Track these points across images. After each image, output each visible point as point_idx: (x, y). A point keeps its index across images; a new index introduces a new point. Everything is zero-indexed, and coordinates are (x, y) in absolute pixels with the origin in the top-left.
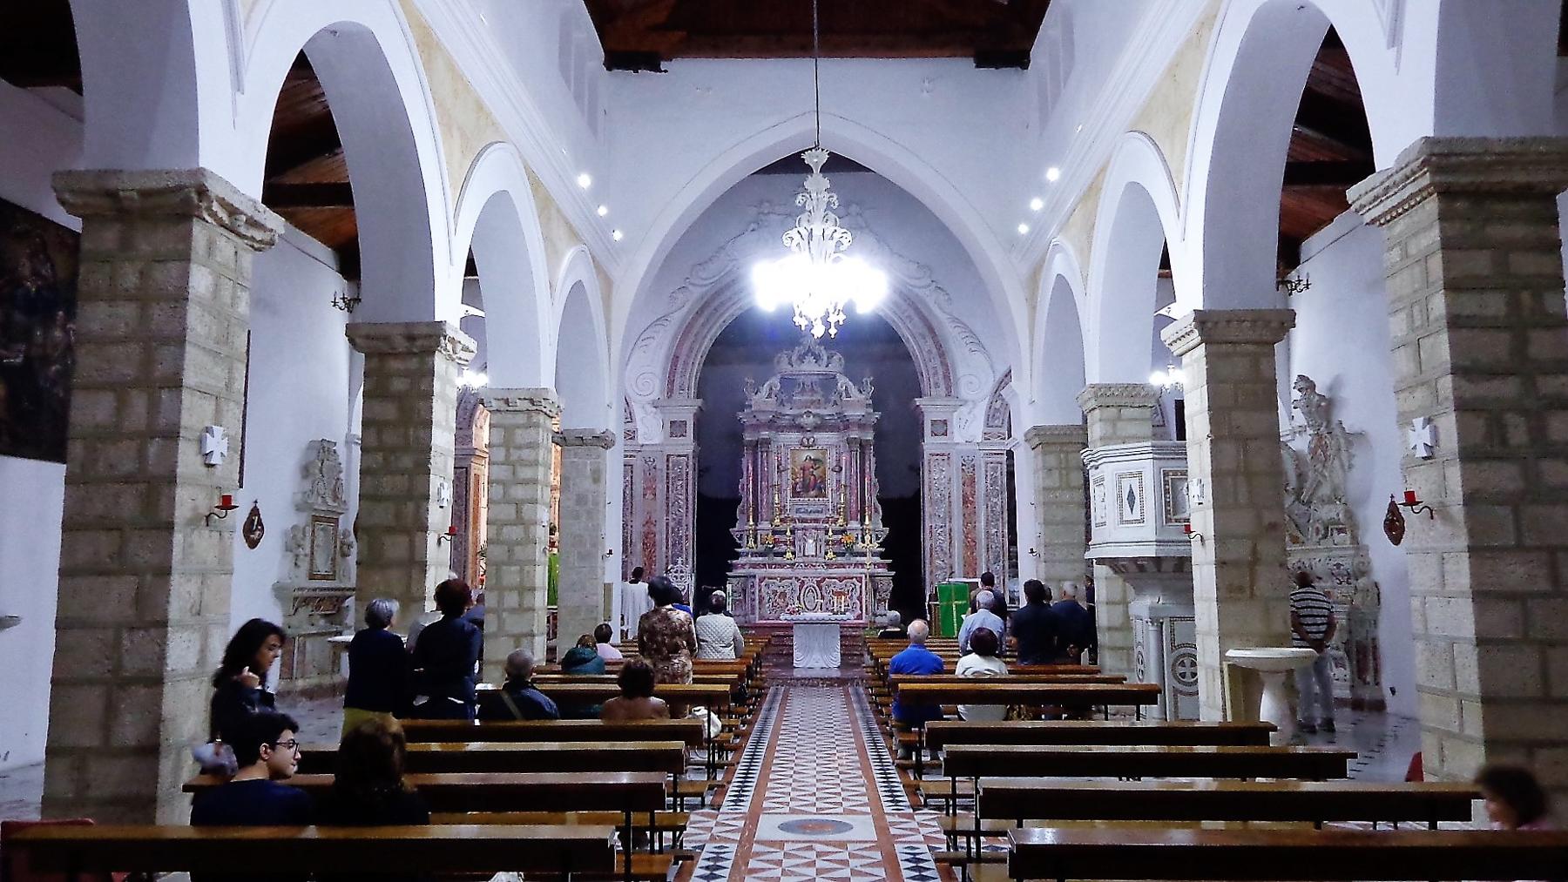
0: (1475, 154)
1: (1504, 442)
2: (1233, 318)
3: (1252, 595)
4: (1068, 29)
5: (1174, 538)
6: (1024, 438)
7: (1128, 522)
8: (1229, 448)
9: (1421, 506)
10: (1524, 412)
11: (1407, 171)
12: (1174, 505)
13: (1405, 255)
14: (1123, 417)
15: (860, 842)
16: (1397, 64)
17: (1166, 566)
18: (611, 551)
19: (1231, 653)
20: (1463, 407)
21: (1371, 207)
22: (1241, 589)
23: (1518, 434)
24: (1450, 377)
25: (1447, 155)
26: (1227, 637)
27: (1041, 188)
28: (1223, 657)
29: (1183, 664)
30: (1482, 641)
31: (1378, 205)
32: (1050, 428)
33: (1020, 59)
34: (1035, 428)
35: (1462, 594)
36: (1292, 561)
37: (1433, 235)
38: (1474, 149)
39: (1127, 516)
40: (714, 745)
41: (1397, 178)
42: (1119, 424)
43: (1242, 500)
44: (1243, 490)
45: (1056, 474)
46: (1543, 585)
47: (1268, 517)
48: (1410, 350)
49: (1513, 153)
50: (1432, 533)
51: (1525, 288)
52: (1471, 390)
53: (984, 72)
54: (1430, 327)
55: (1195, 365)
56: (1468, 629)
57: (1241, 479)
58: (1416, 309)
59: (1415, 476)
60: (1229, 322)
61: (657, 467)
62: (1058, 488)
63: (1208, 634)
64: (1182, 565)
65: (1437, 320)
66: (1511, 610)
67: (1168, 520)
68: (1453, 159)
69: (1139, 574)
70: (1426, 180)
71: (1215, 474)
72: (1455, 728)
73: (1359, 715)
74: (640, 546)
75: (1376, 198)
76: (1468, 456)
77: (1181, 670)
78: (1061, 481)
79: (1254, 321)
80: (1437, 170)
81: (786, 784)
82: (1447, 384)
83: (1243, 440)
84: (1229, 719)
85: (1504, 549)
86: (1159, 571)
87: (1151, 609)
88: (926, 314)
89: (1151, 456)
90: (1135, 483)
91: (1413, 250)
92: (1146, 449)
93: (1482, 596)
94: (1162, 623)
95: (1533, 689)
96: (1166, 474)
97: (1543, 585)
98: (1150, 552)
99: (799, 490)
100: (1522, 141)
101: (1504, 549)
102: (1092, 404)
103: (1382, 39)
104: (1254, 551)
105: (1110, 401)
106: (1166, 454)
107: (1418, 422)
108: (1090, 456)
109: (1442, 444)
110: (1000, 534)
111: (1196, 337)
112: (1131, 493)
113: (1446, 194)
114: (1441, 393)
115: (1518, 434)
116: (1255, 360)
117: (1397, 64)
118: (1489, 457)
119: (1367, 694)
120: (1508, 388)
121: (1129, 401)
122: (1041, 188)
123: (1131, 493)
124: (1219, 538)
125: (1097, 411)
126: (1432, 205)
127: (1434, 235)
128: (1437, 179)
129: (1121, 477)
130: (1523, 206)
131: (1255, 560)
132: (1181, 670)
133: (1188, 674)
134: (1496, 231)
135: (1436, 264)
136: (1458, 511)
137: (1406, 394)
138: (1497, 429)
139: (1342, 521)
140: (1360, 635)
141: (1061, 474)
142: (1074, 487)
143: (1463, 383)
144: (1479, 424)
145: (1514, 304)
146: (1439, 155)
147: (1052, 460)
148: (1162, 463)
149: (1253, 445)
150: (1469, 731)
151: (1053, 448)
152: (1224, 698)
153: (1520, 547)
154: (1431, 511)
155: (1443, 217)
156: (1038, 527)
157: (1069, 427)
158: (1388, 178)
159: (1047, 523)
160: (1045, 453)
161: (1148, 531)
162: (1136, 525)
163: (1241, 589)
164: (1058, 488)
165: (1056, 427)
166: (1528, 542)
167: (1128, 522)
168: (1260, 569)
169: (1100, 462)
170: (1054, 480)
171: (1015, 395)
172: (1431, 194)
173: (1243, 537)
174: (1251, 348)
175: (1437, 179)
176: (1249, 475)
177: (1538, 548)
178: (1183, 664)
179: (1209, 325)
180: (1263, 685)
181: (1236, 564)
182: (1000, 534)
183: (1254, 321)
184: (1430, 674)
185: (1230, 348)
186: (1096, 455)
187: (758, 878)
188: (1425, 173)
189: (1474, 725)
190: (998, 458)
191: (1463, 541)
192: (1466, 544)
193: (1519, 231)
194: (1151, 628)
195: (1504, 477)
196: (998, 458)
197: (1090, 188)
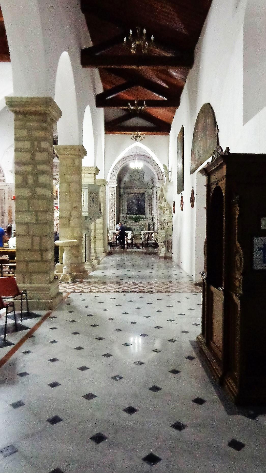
1: (27, 183)
3: (69, 227)
10: (32, 175)
18: (164, 219)
20: (17, 173)
22: (66, 224)
23: (31, 180)
36: (40, 217)
43: (68, 200)
44: (68, 197)
46: (34, 221)
47: (75, 204)
49: (28, 102)
51: (36, 140)
52: (20, 169)
57: (68, 194)
60: (64, 149)
61: (12, 190)
66: (25, 227)
73: (166, 261)
74: (7, 214)
79: (71, 149)
81: (121, 287)
85: (24, 211)
88: (180, 145)
95: (29, 248)
97: (34, 221)
99: (55, 198)
100: (32, 98)
101: (24, 211)
104: (70, 214)
110: (114, 211)
115: (31, 180)
118: (23, 187)
119: (169, 255)
120: (29, 168)
130: (37, 117)
134: (29, 124)
138: (25, 180)
139: (166, 207)
140: (168, 239)
143: (18, 167)
144: (20, 177)
145: (32, 144)
153: (28, 211)
163: (66, 224)
166: (31, 209)
168: (72, 219)
173: (67, 210)
174: (72, 156)
177: (33, 212)
181: (65, 217)
182: (114, 211)
185: (66, 156)
190: (113, 189)
193: (35, 124)
195: (26, 192)
196: (113, 189)
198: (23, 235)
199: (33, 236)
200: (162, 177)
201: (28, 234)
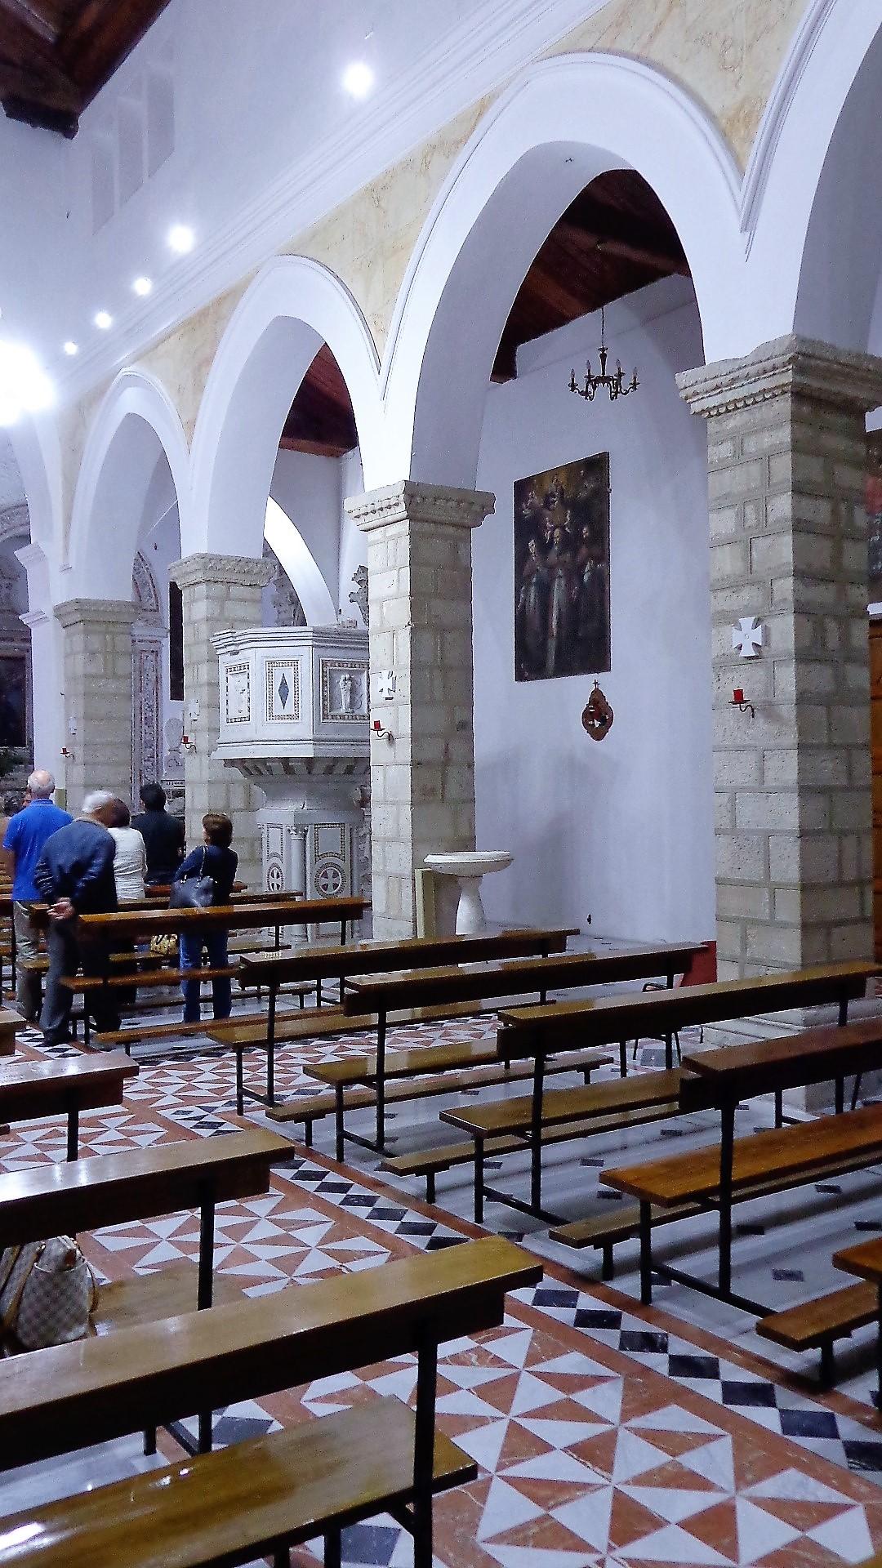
0: (828, 360)
2: (440, 495)
4: (162, 100)
5: (330, 737)
6: (53, 613)
7: (280, 717)
8: (427, 638)
9: (383, 731)
11: (768, 365)
12: (331, 697)
13: (739, 451)
14: (231, 596)
15: (753, 1036)
16: (748, 251)
17: (319, 769)
19: (431, 859)
21: (705, 396)
24: (791, 580)
25: (810, 356)
26: (421, 841)
27: (119, 300)
28: (417, 862)
29: (325, 875)
30: (804, 834)
31: (717, 394)
32: (96, 603)
33: (63, 123)
34: (78, 601)
35: (785, 789)
37: (780, 434)
38: (827, 355)
39: (278, 709)
40: (205, 958)
41: (751, 370)
42: (228, 604)
43: (438, 694)
45: (100, 657)
46: (843, 781)
48: (738, 550)
50: (750, 732)
53: (14, 123)
54: (768, 528)
55: (391, 544)
56: (792, 821)
57: (437, 673)
58: (750, 509)
59: (729, 675)
62: (102, 677)
63: (396, 839)
64: (358, 768)
65: (777, 521)
67: (325, 716)
68: (813, 362)
69: (138, 788)
70: (788, 378)
71: (415, 667)
72: (765, 914)
75: (717, 387)
76: (804, 657)
77: (324, 881)
78: (105, 669)
79: (459, 502)
80: (800, 370)
82: (786, 587)
83: (441, 630)
84: (421, 935)
86: (309, 773)
87: (297, 816)
89: (310, 642)
90: (289, 673)
91: (751, 446)
92: (306, 634)
93: (807, 790)
94: (306, 831)
96: (324, 664)
98: (307, 752)
101: (818, 747)
102: (199, 577)
103: (736, 223)
104: (447, 750)
105: (220, 576)
106: (325, 641)
107: (748, 622)
108: (231, 639)
109: (773, 645)
111: (401, 511)
112: (284, 684)
113: (800, 395)
114: (777, 597)
116: (455, 549)
117: (748, 251)
121: (240, 578)
122: (119, 300)
123: (284, 684)
124: (415, 737)
125: (203, 587)
126: (784, 406)
127: (785, 435)
128: (798, 379)
129: (271, 663)
131: (447, 761)
132: (324, 881)
133: (330, 886)
135: (783, 467)
136: (789, 711)
137: (728, 592)
141: (105, 660)
142: (121, 677)
146: (804, 355)
147: (96, 642)
148: (321, 651)
149: (449, 636)
150: (782, 916)
151: (96, 627)
152: (414, 907)
153: (831, 746)
154: (753, 710)
155: (796, 419)
156: (73, 724)
157: (119, 604)
158: (740, 368)
159: (88, 717)
160: (87, 633)
161: (304, 727)
162: (290, 721)
164: (102, 677)
165: (104, 602)
167: (280, 717)
169: (241, 647)
170: (97, 668)
171: (41, 557)
172: (784, 393)
174: (451, 530)
175: (798, 379)
176: (445, 669)
178: (325, 875)
179: (418, 499)
180: (460, 889)
183: (459, 502)
184: (736, 866)
186: (237, 639)
187: (15, 1159)
188: (788, 370)
189: (790, 909)
191: (792, 738)
192: (796, 741)
194: (294, 837)
197: (203, 314)
198: (819, 832)
199: (843, 834)
200: (153, 600)
201: (831, 831)
